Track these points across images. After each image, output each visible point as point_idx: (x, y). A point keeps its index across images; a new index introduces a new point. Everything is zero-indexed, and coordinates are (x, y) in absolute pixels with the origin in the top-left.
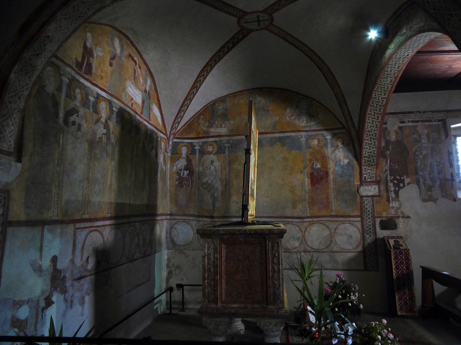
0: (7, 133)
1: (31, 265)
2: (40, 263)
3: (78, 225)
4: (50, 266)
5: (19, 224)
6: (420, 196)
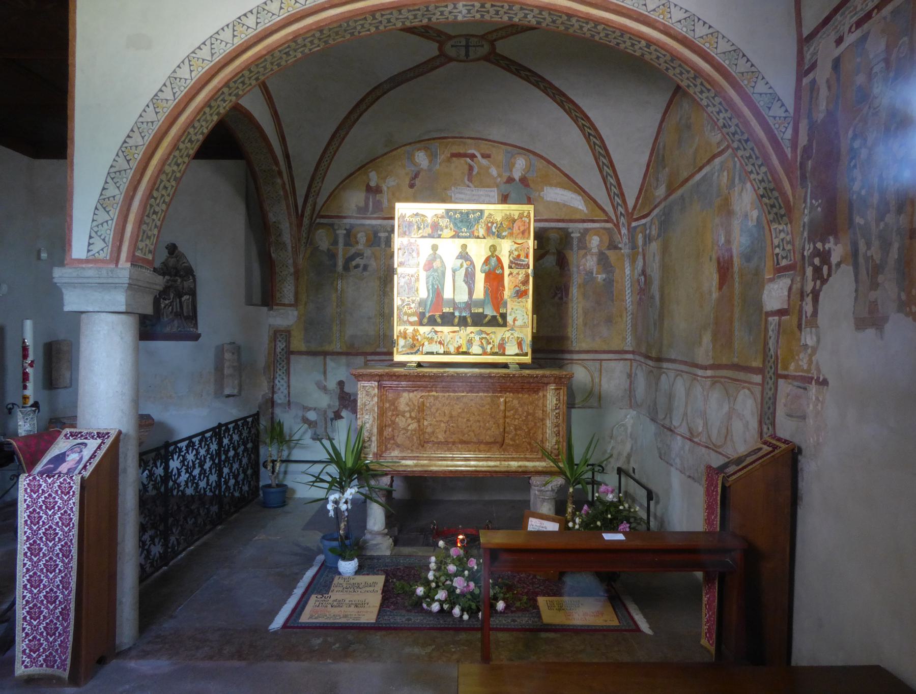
0: (285, 292)
1: (316, 384)
3: (369, 358)
4: (336, 388)
5: (300, 353)
6: (854, 306)
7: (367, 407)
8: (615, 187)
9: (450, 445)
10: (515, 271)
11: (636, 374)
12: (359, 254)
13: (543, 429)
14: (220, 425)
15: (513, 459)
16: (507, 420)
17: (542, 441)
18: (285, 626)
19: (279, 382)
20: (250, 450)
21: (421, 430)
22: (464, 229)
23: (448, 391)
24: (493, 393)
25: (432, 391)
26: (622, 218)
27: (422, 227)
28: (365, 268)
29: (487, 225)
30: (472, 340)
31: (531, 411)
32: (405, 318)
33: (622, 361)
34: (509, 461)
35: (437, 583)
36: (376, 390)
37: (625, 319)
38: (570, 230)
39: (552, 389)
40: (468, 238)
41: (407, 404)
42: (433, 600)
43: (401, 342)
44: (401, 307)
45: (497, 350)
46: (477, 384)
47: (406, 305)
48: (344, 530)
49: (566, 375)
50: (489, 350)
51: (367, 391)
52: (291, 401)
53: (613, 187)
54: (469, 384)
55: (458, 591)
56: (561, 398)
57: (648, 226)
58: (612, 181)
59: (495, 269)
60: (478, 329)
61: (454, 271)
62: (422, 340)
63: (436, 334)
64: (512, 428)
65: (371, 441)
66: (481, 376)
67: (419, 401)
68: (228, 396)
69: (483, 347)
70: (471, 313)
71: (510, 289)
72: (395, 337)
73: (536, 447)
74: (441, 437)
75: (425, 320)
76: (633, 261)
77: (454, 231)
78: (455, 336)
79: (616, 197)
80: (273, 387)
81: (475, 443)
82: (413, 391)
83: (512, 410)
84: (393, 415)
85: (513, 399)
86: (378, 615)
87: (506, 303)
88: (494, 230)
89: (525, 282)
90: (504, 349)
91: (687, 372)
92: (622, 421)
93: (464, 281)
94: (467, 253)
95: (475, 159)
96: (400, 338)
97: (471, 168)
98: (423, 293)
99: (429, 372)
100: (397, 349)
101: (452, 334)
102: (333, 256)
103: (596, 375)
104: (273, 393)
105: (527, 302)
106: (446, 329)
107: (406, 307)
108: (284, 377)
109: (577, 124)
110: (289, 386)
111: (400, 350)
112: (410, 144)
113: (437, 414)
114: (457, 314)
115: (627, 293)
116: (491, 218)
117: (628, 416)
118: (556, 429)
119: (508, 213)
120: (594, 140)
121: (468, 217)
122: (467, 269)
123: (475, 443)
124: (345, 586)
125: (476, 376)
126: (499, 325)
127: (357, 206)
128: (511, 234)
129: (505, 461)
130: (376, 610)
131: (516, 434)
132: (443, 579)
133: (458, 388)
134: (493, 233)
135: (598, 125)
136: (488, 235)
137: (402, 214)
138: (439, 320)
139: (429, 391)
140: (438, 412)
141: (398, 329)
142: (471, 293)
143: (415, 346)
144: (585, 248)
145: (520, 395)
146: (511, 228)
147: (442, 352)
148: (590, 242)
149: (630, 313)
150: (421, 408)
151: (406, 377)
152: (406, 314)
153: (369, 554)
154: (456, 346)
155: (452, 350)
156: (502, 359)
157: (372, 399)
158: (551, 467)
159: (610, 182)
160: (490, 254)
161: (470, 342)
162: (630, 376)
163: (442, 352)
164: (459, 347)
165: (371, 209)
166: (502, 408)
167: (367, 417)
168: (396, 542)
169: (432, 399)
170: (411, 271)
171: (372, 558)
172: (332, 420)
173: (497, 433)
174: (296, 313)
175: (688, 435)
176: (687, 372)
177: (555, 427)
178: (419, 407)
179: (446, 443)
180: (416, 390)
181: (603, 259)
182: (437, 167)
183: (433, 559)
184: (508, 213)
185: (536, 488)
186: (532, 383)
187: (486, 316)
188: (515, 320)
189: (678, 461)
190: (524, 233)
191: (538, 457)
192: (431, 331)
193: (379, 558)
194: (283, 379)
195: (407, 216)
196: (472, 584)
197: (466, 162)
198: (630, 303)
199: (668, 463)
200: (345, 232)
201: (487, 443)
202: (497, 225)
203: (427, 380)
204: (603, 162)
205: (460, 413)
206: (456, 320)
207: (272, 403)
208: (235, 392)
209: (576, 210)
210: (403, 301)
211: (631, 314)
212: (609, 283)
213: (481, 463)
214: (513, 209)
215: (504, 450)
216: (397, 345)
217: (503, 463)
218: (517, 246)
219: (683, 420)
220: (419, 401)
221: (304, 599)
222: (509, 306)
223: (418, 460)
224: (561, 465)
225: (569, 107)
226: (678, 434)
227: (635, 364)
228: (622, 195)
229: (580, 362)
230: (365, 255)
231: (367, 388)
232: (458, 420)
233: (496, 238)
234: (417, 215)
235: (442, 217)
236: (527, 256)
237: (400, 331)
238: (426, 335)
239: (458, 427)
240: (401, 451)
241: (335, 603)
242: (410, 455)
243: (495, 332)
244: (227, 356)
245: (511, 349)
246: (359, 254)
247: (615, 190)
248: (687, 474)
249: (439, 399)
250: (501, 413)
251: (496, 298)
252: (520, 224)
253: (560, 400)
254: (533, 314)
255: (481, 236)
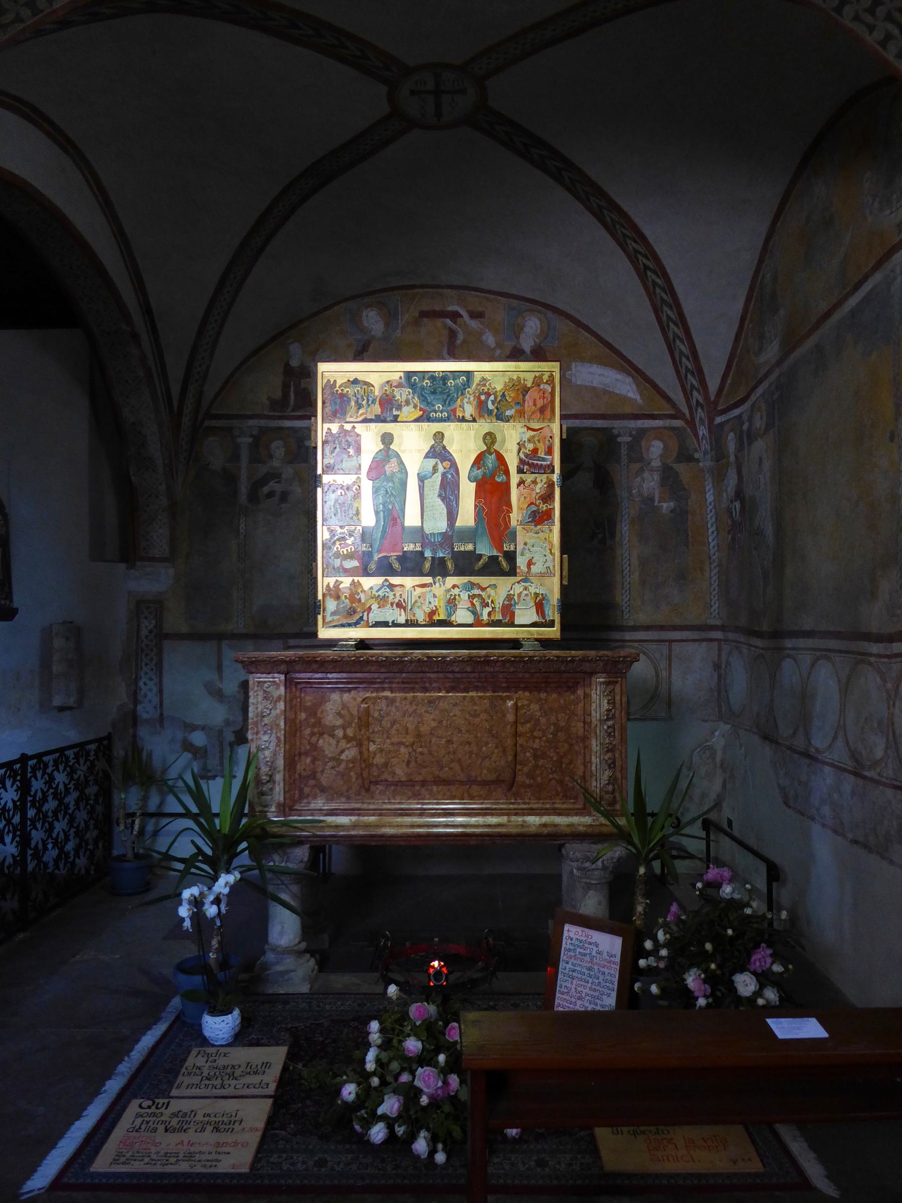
2: (220, 686)
7: (266, 721)
8: (688, 359)
9: (417, 788)
10: (529, 478)
11: (728, 663)
12: (275, 476)
13: (584, 757)
14: (24, 758)
15: (532, 812)
16: (520, 741)
17: (584, 777)
18: (57, 1184)
19: (145, 684)
20: (92, 797)
21: (364, 761)
22: (439, 406)
23: (413, 690)
24: (494, 692)
25: (384, 689)
26: (700, 410)
27: (364, 403)
28: (284, 497)
29: (479, 398)
30: (455, 599)
31: (562, 724)
32: (337, 563)
33: (705, 643)
34: (524, 815)
35: (382, 1078)
36: (282, 689)
37: (707, 574)
38: (616, 432)
39: (601, 683)
40: (445, 421)
41: (339, 714)
42: (374, 1118)
43: (331, 605)
44: (330, 544)
45: (499, 617)
46: (465, 675)
47: (339, 539)
48: (218, 951)
49: (625, 657)
50: (485, 617)
51: (265, 691)
52: (165, 714)
53: (684, 360)
54: (450, 675)
55: (424, 1100)
56: (618, 698)
57: (745, 417)
58: (682, 347)
59: (493, 476)
60: (465, 579)
61: (422, 479)
62: (367, 600)
63: (392, 591)
64: (528, 754)
65: (274, 782)
66: (470, 660)
67: (359, 707)
68: (61, 709)
69: (474, 612)
70: (453, 551)
71: (520, 508)
72: (320, 597)
73: (573, 788)
74: (401, 772)
75: (373, 566)
76: (719, 477)
77: (421, 409)
78: (424, 594)
79: (689, 376)
80: (135, 694)
81: (462, 783)
82: (349, 690)
83: (528, 722)
84: (313, 734)
85: (531, 702)
86: (258, 1151)
87: (514, 534)
88: (491, 406)
89: (547, 497)
90: (513, 615)
91: (841, 651)
92: (707, 741)
93: (440, 496)
94: (444, 447)
95: (459, 320)
96: (328, 599)
97: (453, 334)
98: (368, 519)
99: (377, 654)
100: (324, 618)
101: (419, 591)
102: (231, 479)
103: (663, 664)
104: (136, 702)
105: (551, 531)
106: (409, 582)
107: (338, 543)
108: (154, 677)
109: (624, 250)
110: (161, 691)
111: (329, 619)
112: (354, 297)
113: (393, 732)
114: (428, 554)
115: (710, 531)
116: (485, 385)
117: (717, 733)
118: (609, 755)
119: (515, 378)
120: (654, 277)
121: (445, 384)
122: (444, 475)
123: (462, 783)
124: (205, 1074)
125: (463, 661)
126: (503, 573)
127: (269, 398)
128: (521, 414)
129: (516, 814)
130: (254, 1139)
131: (536, 766)
132: (395, 1066)
133: (431, 683)
134: (490, 413)
135: (660, 250)
136: (481, 416)
137: (329, 381)
138: (396, 565)
139: (377, 690)
140: (395, 727)
141: (324, 582)
142: (452, 516)
143: (355, 612)
144: (641, 459)
145: (543, 695)
146: (521, 403)
147: (403, 622)
148: (648, 450)
149: (715, 564)
150: (365, 720)
151: (338, 665)
152: (337, 555)
153: (270, 992)
154: (428, 610)
155: (421, 617)
156: (509, 632)
157: (275, 705)
158: (601, 825)
159: (680, 349)
160: (485, 448)
161: (452, 603)
162: (717, 667)
163: (403, 622)
164: (433, 613)
165: (292, 402)
166: (510, 718)
167: (266, 738)
168: (323, 964)
169: (383, 704)
170: (348, 480)
171: (275, 998)
172: (231, 745)
173: (503, 763)
174: (171, 571)
175: (849, 764)
176: (841, 651)
177: (608, 751)
178: (359, 718)
179: (411, 783)
180: (355, 688)
181: (669, 477)
182: (398, 333)
183: (375, 1026)
184: (515, 378)
185: (575, 864)
186: (565, 672)
187: (481, 556)
188: (530, 564)
189: (826, 810)
190: (544, 411)
191: (576, 806)
192: (383, 585)
193: (286, 999)
194: (151, 679)
195: (338, 385)
196: (454, 1079)
197: (445, 325)
198: (716, 548)
199: (802, 814)
200: (250, 440)
201: (484, 783)
202: (496, 398)
203: (373, 669)
204: (667, 315)
205: (433, 729)
206: (427, 565)
207: (134, 719)
208: (71, 701)
209: (624, 399)
210: (331, 531)
211: (718, 565)
212: (681, 515)
213: (473, 820)
214: (525, 370)
215: (516, 795)
216: (324, 610)
217: (513, 818)
218: (532, 433)
219: (835, 738)
220: (359, 707)
221: (118, 1107)
222: (520, 539)
223: (359, 815)
224: (622, 821)
225: (612, 219)
226: (825, 763)
227: (726, 648)
228: (699, 372)
229: (636, 644)
230: (283, 476)
231: (266, 685)
232: (431, 741)
233: (494, 420)
234: (356, 382)
235: (399, 385)
236: (550, 451)
237: (328, 586)
238: (374, 593)
239: (430, 753)
240: (327, 799)
241: (174, 1122)
242: (346, 806)
243: (495, 586)
244: (58, 643)
245: (526, 615)
246: (275, 476)
247: (687, 363)
248: (850, 836)
249: (398, 704)
250: (509, 727)
251: (498, 525)
252: (537, 396)
253: (614, 703)
254: (563, 552)
255: (468, 417)
